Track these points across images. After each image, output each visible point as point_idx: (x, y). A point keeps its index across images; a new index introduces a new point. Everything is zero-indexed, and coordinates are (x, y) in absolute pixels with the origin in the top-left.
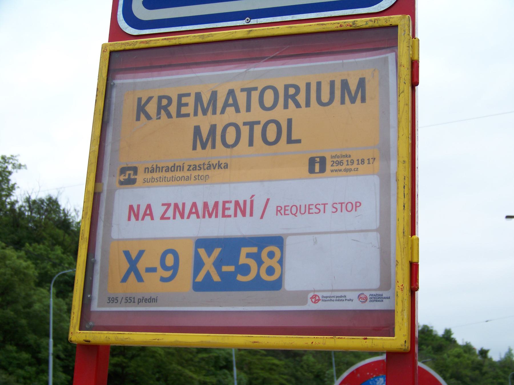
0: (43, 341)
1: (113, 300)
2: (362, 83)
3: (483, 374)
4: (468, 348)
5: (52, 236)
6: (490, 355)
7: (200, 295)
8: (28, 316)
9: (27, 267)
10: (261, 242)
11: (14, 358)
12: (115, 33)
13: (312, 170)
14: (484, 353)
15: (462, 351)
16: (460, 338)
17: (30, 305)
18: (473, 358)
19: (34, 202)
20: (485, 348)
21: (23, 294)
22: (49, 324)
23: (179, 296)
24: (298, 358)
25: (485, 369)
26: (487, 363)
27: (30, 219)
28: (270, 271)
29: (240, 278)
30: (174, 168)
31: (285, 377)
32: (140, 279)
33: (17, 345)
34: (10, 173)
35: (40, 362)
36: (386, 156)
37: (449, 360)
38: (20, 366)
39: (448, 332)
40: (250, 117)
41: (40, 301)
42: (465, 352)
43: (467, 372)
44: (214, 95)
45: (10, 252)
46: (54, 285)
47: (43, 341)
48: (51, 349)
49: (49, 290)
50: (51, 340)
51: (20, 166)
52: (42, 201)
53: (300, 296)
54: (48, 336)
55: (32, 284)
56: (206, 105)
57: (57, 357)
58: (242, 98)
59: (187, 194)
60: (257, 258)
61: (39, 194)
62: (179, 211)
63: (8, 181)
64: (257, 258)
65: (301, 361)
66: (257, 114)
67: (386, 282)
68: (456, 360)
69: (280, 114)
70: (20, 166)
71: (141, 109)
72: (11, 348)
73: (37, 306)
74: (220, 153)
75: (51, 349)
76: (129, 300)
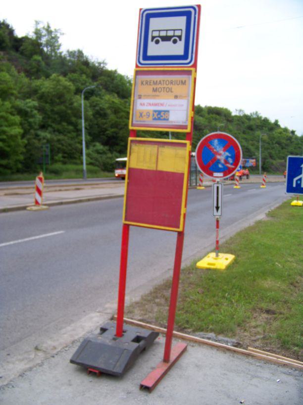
0: (79, 121)
1: (137, 121)
2: (185, 81)
3: (292, 142)
4: (286, 130)
5: (81, 69)
6: (296, 133)
7: (154, 121)
8: (71, 109)
9: (70, 85)
10: (165, 111)
11: (66, 129)
12: (137, 66)
13: (175, 98)
14: (293, 132)
15: (282, 131)
16: (282, 125)
17: (72, 104)
18: (288, 134)
19: (71, 52)
20: (294, 130)
21: (69, 98)
22: (81, 112)
23: (149, 121)
24: (201, 131)
25: (293, 140)
26: (294, 137)
27: (70, 61)
28: (167, 117)
29: (161, 118)
30: (149, 96)
31: (194, 140)
32: (142, 117)
33: (67, 122)
34: (58, 37)
35: (78, 131)
36: (188, 96)
37: (275, 135)
38: (69, 132)
39: (277, 121)
40: (163, 86)
41: (77, 102)
42: (284, 131)
43: (284, 141)
44: (157, 81)
45: (61, 78)
46: (84, 94)
47: (79, 121)
48: (83, 125)
49: (81, 96)
50: (83, 121)
51: (63, 34)
52: (75, 52)
53: (172, 122)
54: (81, 118)
55: (73, 94)
56: (155, 83)
57: (86, 128)
58: (162, 82)
59: (152, 101)
60: (164, 114)
61: (74, 48)
62: (150, 104)
63: (58, 42)
64: (164, 114)
65: (203, 132)
66: (165, 86)
67: (187, 120)
68: (279, 135)
69: (170, 86)
70: (63, 34)
71: (142, 83)
72: (64, 124)
73: (75, 104)
74: (157, 93)
75: (83, 125)
76: (140, 121)
